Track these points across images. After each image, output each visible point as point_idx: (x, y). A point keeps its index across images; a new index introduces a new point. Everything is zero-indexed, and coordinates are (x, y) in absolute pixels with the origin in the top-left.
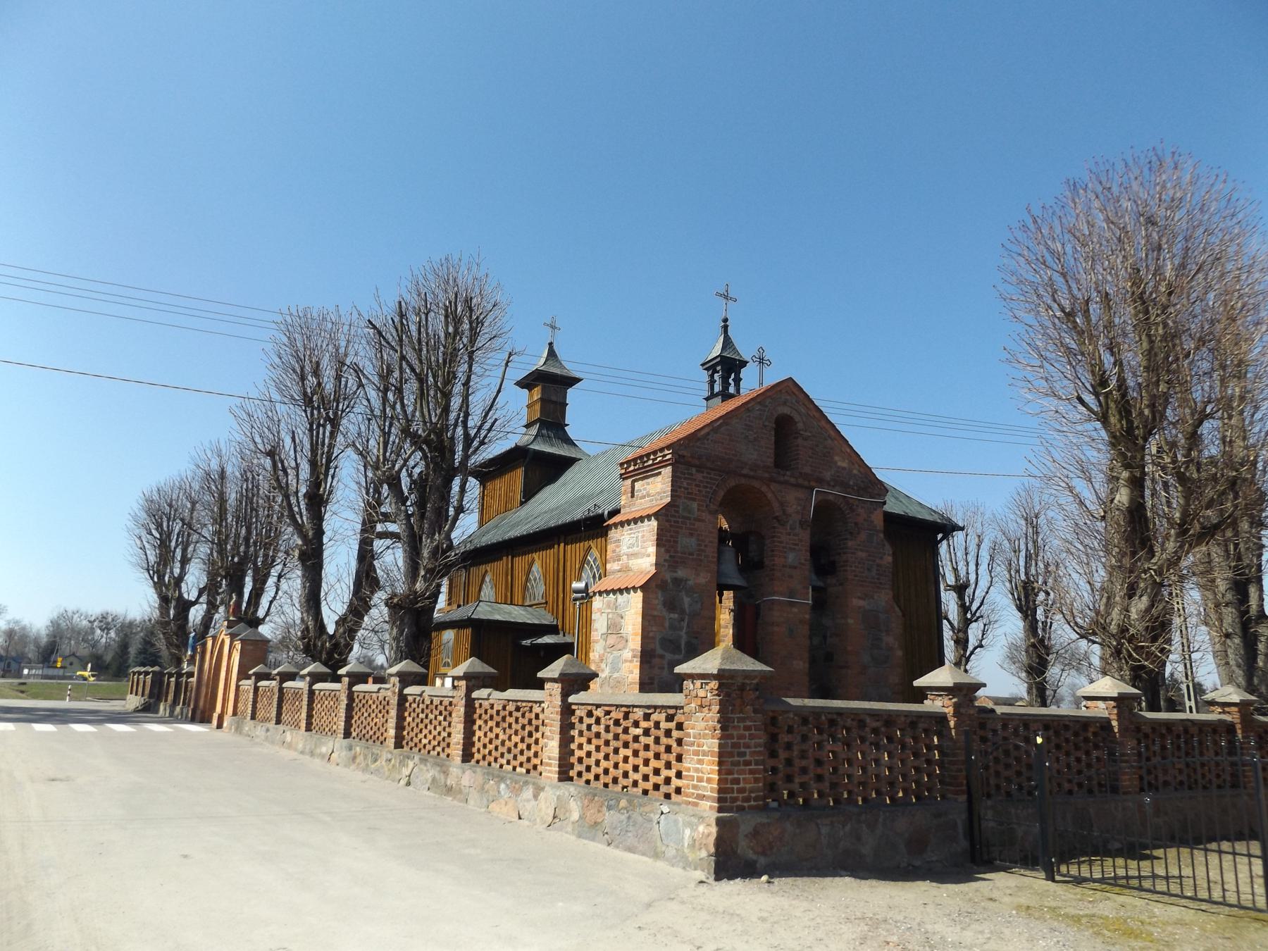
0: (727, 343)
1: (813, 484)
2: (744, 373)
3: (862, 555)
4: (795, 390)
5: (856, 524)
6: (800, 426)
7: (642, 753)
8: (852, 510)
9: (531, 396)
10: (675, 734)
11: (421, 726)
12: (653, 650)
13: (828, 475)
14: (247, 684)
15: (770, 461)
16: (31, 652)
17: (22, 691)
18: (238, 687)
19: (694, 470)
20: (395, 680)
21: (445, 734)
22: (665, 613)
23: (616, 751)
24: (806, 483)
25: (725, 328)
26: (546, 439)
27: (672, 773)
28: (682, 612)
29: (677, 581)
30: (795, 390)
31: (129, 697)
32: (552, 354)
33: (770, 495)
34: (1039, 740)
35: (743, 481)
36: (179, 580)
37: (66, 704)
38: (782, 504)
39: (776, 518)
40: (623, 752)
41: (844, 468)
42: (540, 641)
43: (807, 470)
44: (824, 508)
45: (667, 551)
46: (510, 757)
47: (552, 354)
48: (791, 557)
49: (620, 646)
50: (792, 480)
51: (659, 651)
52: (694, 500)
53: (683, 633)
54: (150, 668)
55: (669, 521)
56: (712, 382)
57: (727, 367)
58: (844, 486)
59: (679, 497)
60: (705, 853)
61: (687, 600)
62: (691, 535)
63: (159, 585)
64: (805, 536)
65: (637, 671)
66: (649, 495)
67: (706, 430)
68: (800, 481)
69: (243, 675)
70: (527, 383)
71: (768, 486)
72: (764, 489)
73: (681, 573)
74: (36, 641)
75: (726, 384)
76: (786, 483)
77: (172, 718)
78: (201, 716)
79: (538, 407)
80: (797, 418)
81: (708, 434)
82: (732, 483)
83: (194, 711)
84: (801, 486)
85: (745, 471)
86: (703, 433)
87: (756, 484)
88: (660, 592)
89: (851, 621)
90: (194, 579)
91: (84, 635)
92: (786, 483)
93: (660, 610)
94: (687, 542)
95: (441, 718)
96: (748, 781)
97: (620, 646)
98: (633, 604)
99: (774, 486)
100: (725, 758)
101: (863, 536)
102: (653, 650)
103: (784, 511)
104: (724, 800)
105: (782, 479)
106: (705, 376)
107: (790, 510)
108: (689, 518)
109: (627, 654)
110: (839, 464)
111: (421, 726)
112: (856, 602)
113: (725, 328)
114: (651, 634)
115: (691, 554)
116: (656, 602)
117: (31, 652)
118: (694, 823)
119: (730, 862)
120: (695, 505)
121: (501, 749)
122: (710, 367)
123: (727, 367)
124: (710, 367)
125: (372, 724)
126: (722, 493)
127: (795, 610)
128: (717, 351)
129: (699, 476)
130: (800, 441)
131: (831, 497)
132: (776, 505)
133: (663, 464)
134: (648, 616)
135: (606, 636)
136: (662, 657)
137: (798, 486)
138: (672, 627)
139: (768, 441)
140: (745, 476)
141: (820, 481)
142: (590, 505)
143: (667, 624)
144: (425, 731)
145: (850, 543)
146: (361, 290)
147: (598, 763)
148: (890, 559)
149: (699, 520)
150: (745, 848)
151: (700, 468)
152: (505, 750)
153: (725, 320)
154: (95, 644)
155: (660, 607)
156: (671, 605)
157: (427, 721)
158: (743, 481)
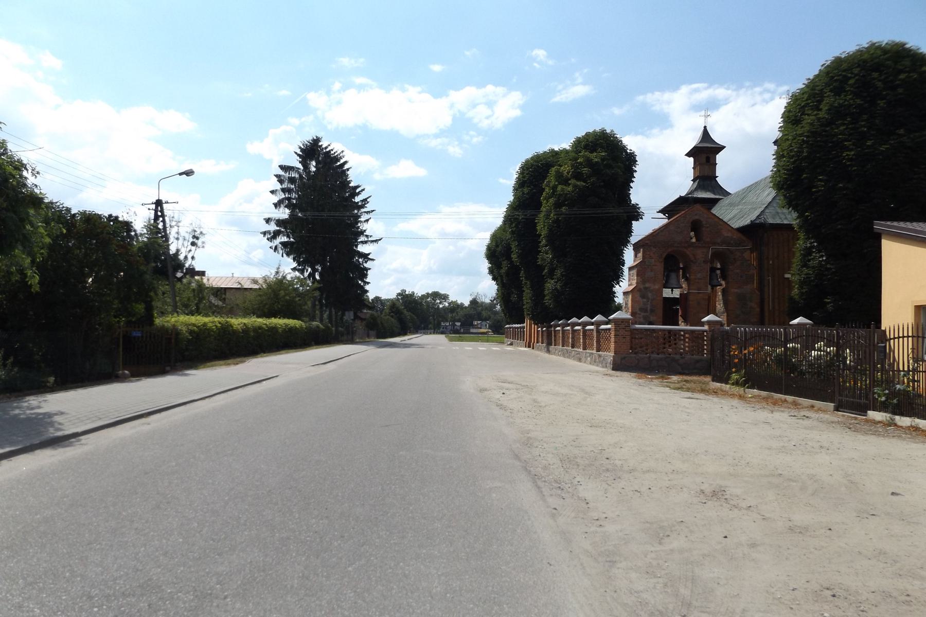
29: (646, 288)
61: (650, 295)
73: (647, 285)
156: (643, 297)
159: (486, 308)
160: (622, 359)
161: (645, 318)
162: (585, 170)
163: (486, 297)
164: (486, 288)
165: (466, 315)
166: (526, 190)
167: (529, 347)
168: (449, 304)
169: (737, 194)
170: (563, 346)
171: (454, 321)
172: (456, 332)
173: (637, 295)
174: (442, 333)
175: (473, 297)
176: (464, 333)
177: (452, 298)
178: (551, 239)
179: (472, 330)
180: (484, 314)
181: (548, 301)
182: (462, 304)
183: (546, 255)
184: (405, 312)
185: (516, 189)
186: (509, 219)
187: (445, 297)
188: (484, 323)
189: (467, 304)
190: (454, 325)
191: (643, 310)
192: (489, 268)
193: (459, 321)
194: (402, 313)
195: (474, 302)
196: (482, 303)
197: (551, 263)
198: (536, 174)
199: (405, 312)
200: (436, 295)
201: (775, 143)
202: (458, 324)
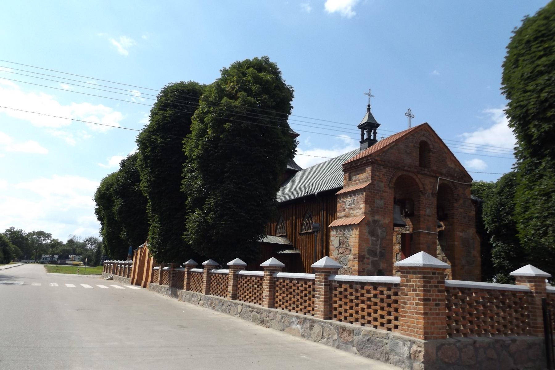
1: (437, 175)
2: (378, 130)
3: (461, 210)
4: (428, 129)
5: (458, 195)
6: (431, 146)
7: (373, 307)
8: (456, 189)
10: (393, 297)
11: (245, 289)
12: (364, 255)
13: (444, 171)
15: (417, 163)
18: (153, 270)
19: (382, 167)
21: (258, 294)
22: (369, 237)
23: (357, 305)
24: (434, 175)
25: (369, 109)
27: (392, 317)
28: (377, 237)
29: (375, 222)
30: (428, 129)
31: (103, 273)
33: (417, 180)
35: (405, 173)
38: (423, 185)
39: (421, 191)
40: (361, 306)
41: (452, 168)
42: (285, 252)
43: (435, 168)
44: (443, 188)
45: (370, 207)
46: (295, 306)
48: (428, 211)
49: (347, 253)
50: (428, 173)
51: (367, 256)
52: (382, 182)
53: (378, 247)
55: (370, 194)
56: (363, 135)
57: (370, 126)
58: (453, 177)
59: (375, 180)
61: (379, 231)
62: (381, 199)
64: (434, 201)
65: (357, 265)
66: (359, 180)
67: (388, 147)
68: (432, 174)
71: (417, 176)
72: (415, 177)
73: (376, 218)
75: (369, 135)
76: (426, 174)
80: (429, 142)
81: (388, 149)
82: (400, 174)
83: (133, 280)
84: (432, 176)
85: (406, 168)
86: (386, 149)
87: (411, 175)
88: (368, 226)
89: (456, 243)
92: (426, 174)
93: (367, 235)
94: (379, 202)
95: (256, 286)
97: (347, 253)
99: (420, 176)
101: (461, 201)
102: (364, 255)
103: (424, 188)
105: (423, 172)
106: (359, 131)
107: (427, 188)
108: (380, 191)
109: (350, 257)
110: (450, 165)
111: (245, 289)
112: (459, 234)
113: (369, 109)
114: (363, 247)
115: (381, 208)
116: (366, 231)
120: (382, 185)
121: (289, 302)
122: (362, 127)
123: (370, 126)
124: (362, 127)
125: (220, 288)
126: (395, 179)
127: (430, 237)
128: (366, 120)
129: (384, 170)
130: (431, 154)
131: (446, 182)
132: (421, 186)
135: (338, 248)
136: (368, 258)
137: (431, 176)
138: (373, 244)
139: (416, 154)
140: (406, 171)
141: (441, 174)
142: (308, 190)
143: (370, 243)
144: (247, 292)
145: (455, 205)
147: (346, 311)
148: (474, 213)
149: (385, 192)
151: (385, 166)
152: (291, 302)
153: (369, 106)
155: (367, 234)
156: (372, 233)
157: (248, 287)
158: (405, 173)
159: (80, 246)
160: (438, 348)
161: (374, 264)
162: (255, 88)
163: (81, 238)
164: (87, 227)
165: (64, 250)
166: (169, 112)
167: (138, 284)
168: (52, 241)
169: (307, 169)
170: (208, 293)
171: (53, 254)
172: (53, 262)
173: (366, 230)
174: (42, 263)
175: (70, 238)
176: (60, 264)
177: (54, 237)
178: (205, 162)
179: (67, 262)
180: (78, 250)
181: (190, 237)
182: (61, 243)
183: (192, 180)
184: (11, 244)
185: (154, 114)
186: (146, 140)
187: (48, 236)
188: (77, 257)
189: (65, 242)
190: (53, 257)
191: (372, 252)
192: (96, 209)
193: (58, 255)
194: (7, 246)
195: (71, 242)
196: (77, 242)
197: (199, 191)
198: (177, 106)
199: (11, 244)
200: (41, 234)
201: (503, 66)
202: (56, 256)
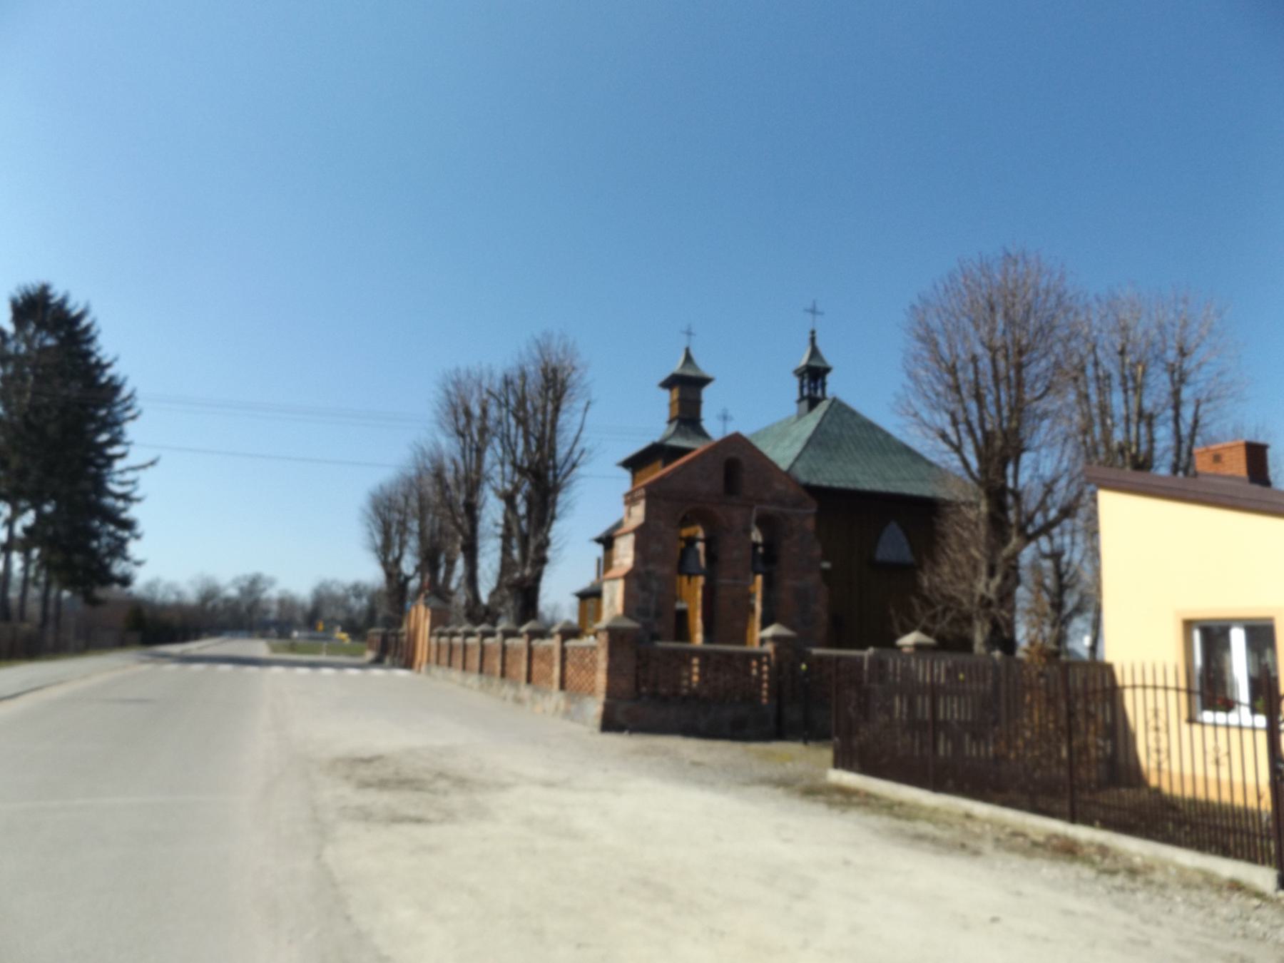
0: (815, 353)
9: (671, 396)
14: (434, 640)
16: (299, 618)
17: (293, 648)
20: (526, 637)
25: (813, 340)
26: (685, 435)
29: (649, 573)
32: (688, 359)
34: (804, 667)
36: (397, 561)
37: (322, 657)
47: (688, 359)
54: (372, 629)
56: (802, 387)
60: (596, 721)
63: (385, 564)
69: (431, 634)
70: (669, 383)
73: (651, 567)
74: (303, 607)
77: (394, 665)
78: (408, 664)
79: (676, 406)
90: (409, 565)
91: (340, 602)
96: (625, 684)
98: (619, 587)
100: (611, 672)
104: (610, 693)
113: (813, 340)
117: (299, 618)
118: (594, 707)
119: (609, 724)
122: (800, 373)
128: (804, 360)
133: (640, 498)
134: (628, 595)
146: (497, 354)
150: (619, 718)
153: (813, 332)
154: (350, 611)
156: (644, 587)
